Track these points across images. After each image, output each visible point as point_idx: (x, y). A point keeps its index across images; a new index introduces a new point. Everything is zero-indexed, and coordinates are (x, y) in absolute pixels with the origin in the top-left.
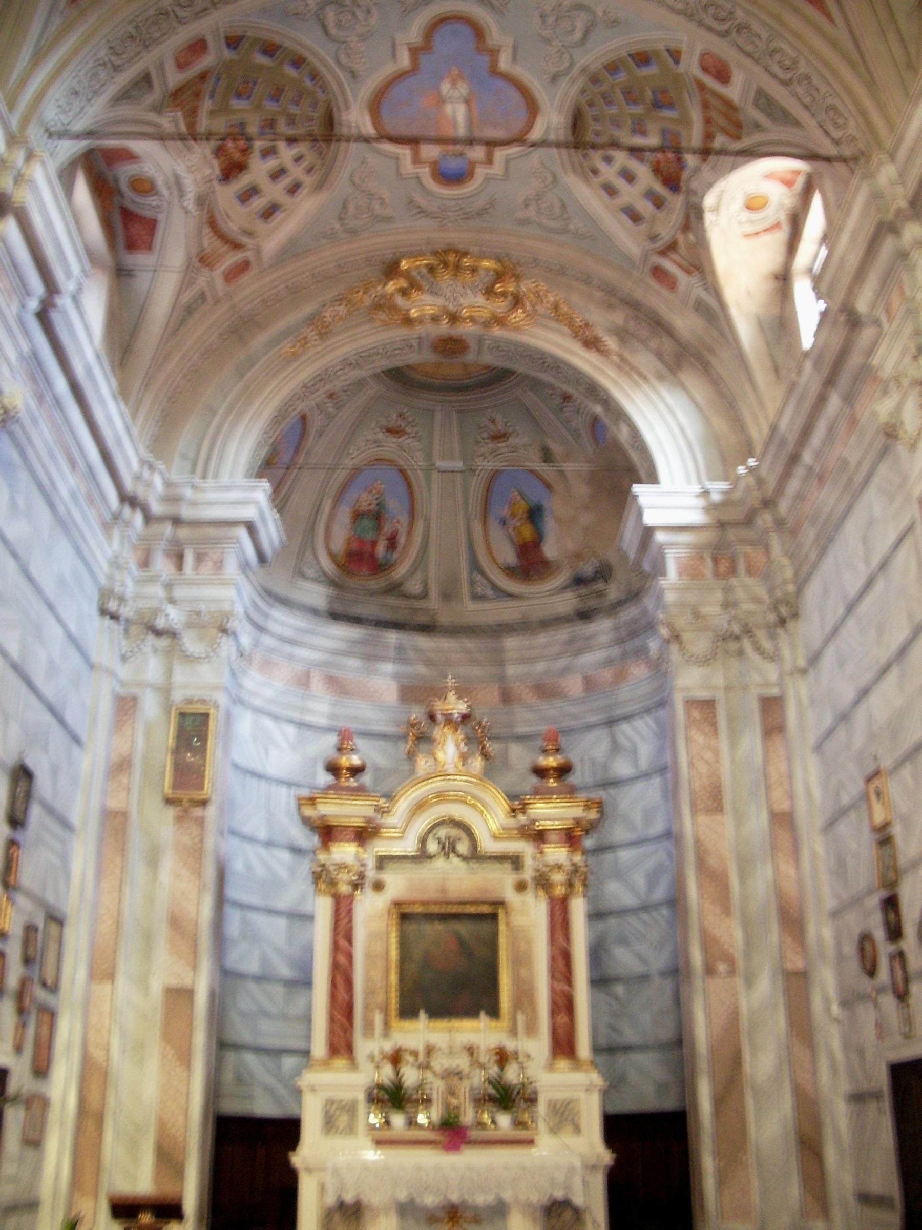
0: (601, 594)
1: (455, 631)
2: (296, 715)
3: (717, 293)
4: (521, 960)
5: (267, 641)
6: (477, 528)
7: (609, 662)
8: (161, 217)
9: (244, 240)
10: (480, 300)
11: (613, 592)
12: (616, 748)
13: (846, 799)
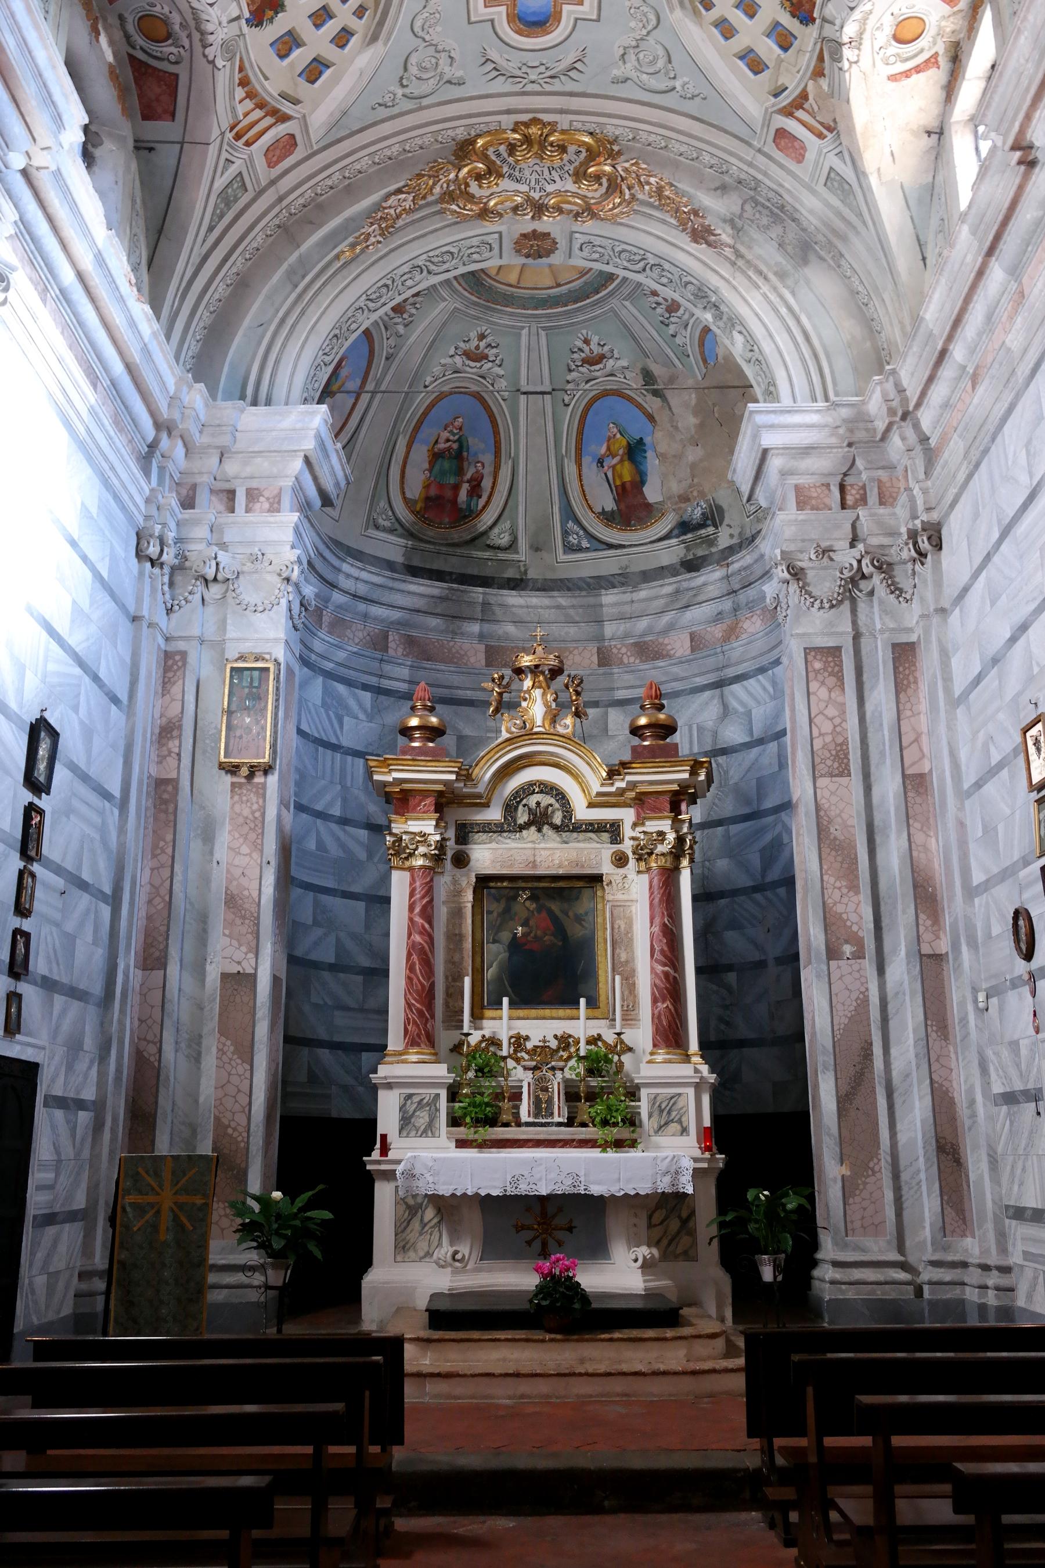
0: (710, 541)
1: (546, 586)
2: (373, 681)
3: (855, 163)
4: (622, 940)
5: (338, 597)
6: (571, 468)
7: (719, 617)
8: (182, 71)
9: (286, 108)
10: (570, 185)
11: (724, 539)
12: (726, 711)
13: (996, 757)
